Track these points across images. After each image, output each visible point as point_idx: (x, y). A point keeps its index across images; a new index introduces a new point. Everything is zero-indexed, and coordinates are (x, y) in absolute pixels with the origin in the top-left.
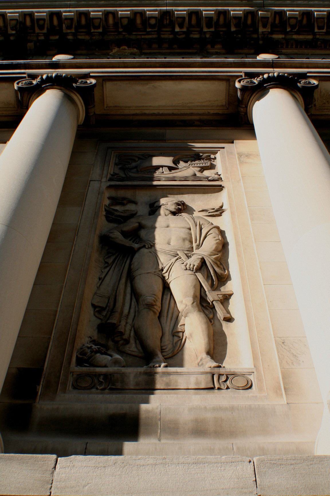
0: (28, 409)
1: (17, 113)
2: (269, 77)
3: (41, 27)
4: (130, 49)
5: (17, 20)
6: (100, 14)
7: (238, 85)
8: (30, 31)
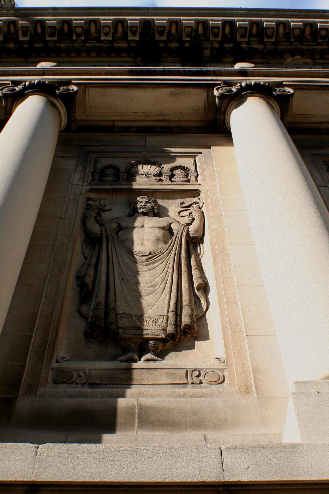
1: (206, 118)
2: (247, 84)
3: (216, 35)
4: (303, 59)
5: (192, 27)
6: (274, 24)
7: (216, 93)
8: (202, 38)
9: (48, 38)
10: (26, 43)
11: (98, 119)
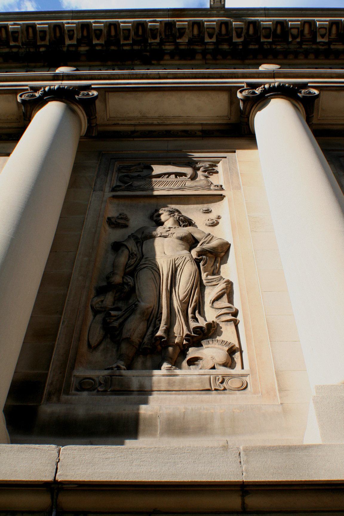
0: (34, 412)
7: (239, 95)
9: (262, 40)
10: (239, 45)
11: (330, 123)
